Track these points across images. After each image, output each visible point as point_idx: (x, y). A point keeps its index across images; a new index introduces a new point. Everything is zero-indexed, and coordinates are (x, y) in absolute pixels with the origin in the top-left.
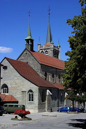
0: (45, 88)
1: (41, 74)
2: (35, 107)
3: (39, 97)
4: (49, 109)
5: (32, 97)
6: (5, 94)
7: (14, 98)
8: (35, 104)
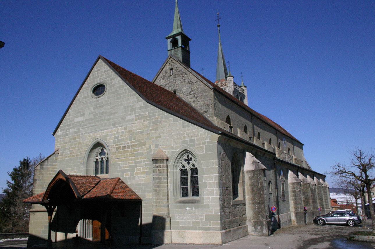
0: (240, 146)
1: (215, 118)
2: (208, 218)
3: (221, 177)
4: (261, 225)
5: (195, 181)
6: (99, 175)
7: (126, 188)
8: (208, 206)
